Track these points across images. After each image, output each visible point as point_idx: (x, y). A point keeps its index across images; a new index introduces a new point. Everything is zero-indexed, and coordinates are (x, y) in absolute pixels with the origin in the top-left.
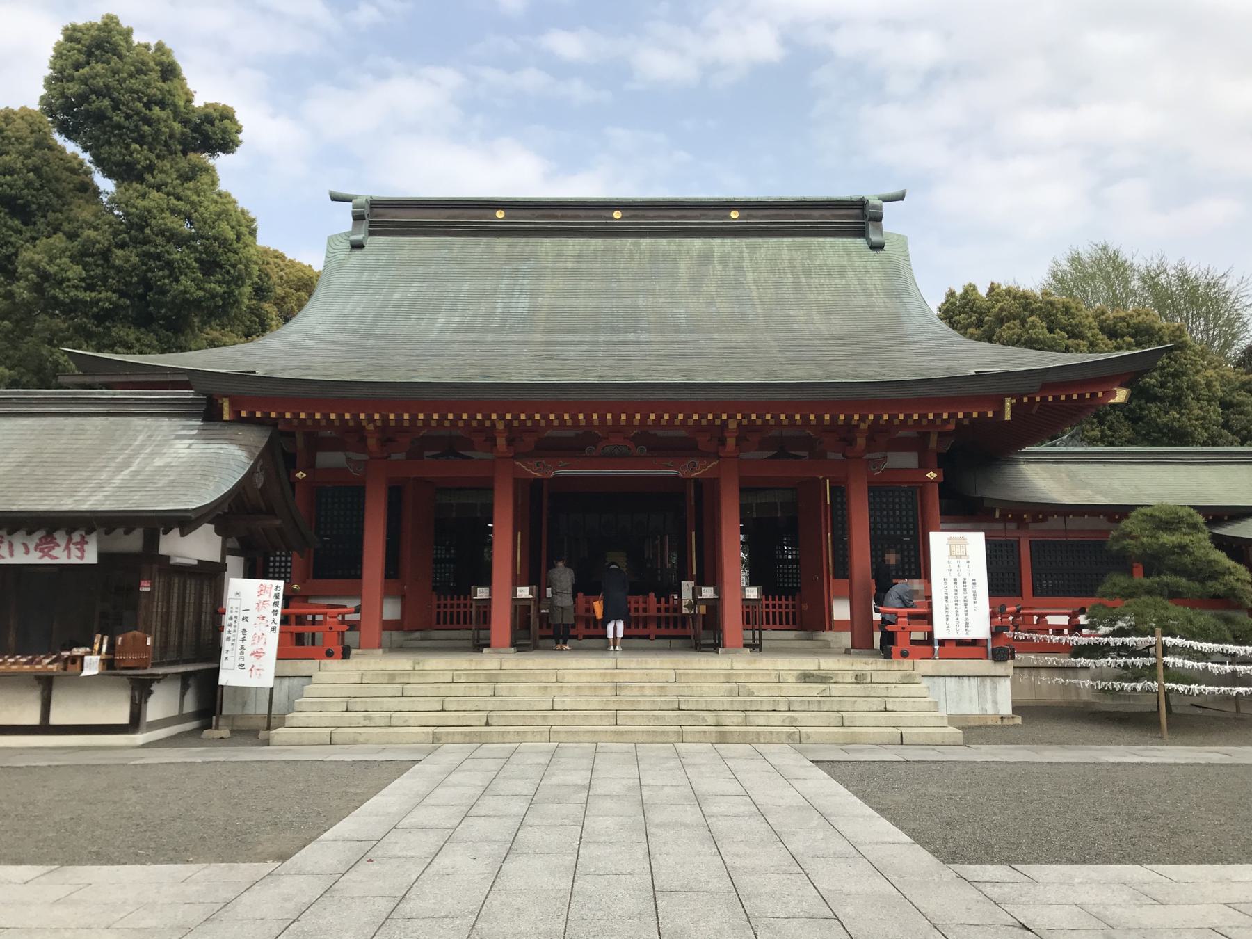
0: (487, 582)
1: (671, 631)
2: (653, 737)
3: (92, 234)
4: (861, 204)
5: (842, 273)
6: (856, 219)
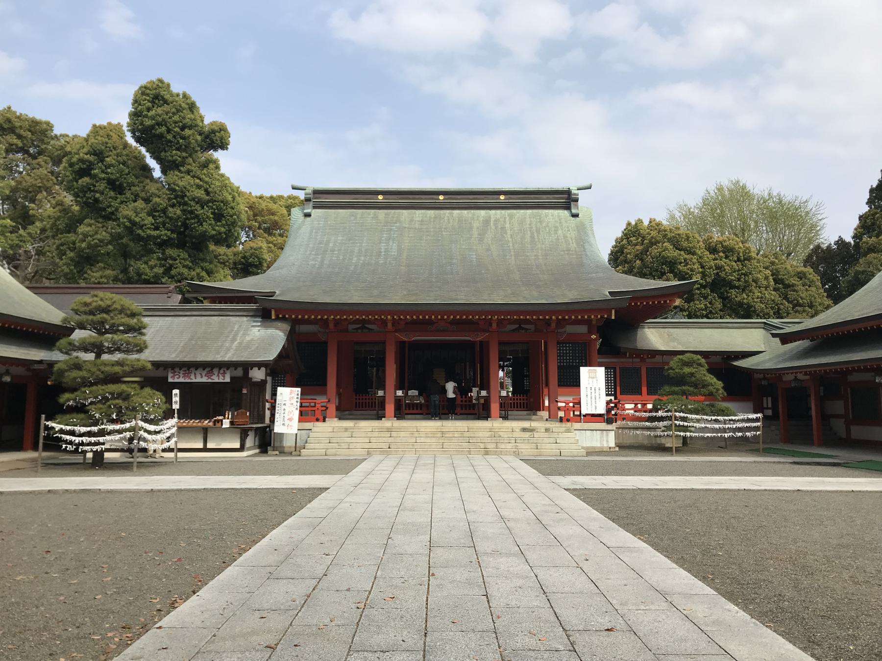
0: (383, 388)
1: (468, 411)
2: (458, 452)
3: (157, 200)
4: (568, 192)
5: (556, 231)
6: (565, 200)
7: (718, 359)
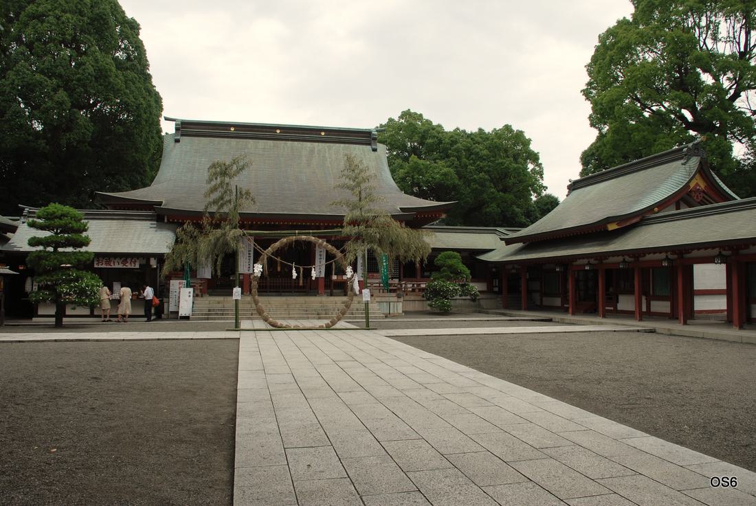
7: (465, 254)
